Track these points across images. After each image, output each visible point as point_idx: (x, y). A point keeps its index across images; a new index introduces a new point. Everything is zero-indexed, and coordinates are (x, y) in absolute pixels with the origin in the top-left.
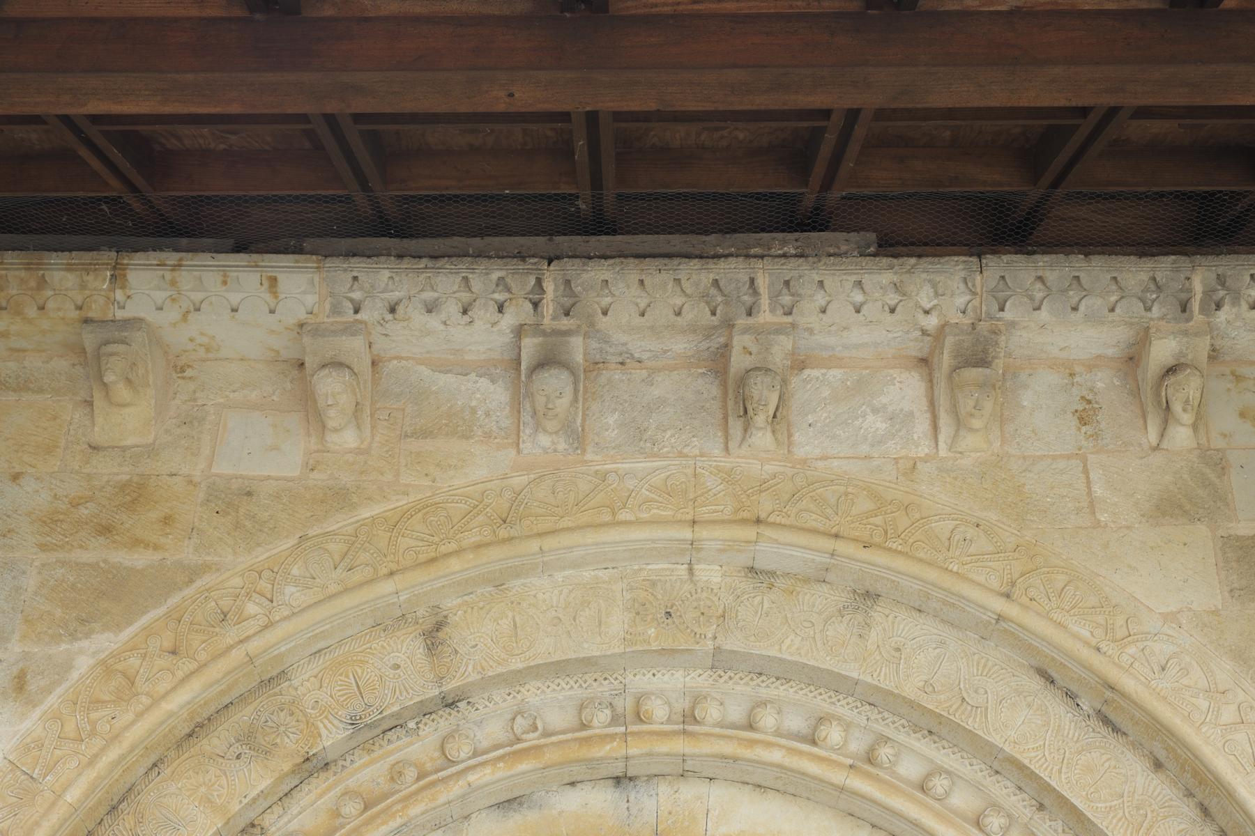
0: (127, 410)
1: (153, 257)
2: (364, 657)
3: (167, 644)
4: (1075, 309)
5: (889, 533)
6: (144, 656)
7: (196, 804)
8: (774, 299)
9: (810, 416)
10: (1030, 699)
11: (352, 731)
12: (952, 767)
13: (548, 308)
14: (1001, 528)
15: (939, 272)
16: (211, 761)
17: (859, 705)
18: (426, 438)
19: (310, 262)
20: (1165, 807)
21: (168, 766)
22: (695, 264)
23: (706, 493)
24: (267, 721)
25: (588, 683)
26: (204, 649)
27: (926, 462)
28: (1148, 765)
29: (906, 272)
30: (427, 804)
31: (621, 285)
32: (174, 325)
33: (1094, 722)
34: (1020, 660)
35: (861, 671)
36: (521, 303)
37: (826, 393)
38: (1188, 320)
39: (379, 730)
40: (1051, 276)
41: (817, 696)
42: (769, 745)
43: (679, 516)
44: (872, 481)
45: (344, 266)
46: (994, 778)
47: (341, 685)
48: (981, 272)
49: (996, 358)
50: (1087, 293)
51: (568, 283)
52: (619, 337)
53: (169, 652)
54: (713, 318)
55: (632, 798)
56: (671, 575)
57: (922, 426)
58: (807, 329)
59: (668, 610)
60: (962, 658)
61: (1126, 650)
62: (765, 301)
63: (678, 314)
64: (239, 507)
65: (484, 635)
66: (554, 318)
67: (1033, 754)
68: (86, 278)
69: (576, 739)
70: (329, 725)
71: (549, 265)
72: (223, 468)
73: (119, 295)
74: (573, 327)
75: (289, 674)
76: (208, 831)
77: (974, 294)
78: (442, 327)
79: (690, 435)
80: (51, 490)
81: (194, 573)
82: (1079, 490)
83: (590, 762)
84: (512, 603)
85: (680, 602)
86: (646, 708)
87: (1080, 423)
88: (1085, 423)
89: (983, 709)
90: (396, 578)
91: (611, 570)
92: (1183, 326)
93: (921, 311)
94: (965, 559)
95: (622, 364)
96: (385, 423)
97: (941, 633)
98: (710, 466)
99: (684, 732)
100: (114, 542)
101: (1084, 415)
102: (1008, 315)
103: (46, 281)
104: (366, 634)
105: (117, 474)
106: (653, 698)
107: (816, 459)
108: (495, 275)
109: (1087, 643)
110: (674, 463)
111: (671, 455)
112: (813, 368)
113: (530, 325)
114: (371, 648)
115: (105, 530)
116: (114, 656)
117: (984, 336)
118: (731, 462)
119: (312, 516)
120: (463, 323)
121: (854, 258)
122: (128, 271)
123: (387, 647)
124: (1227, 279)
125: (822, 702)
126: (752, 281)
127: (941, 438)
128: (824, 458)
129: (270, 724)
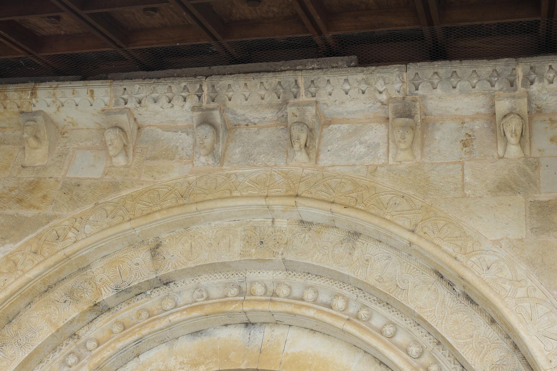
0: (38, 151)
1: (48, 84)
2: (124, 259)
3: (33, 249)
4: (454, 88)
5: (358, 201)
6: (23, 254)
7: (44, 321)
8: (307, 89)
9: (329, 147)
10: (430, 285)
11: (116, 293)
12: (396, 321)
13: (205, 98)
14: (415, 198)
15: (385, 72)
16: (53, 303)
17: (354, 289)
18: (155, 160)
19: (107, 83)
20: (495, 343)
21: (34, 304)
22: (270, 75)
23: (274, 183)
24: (79, 287)
25: (229, 276)
26: (47, 252)
27: (382, 167)
28: (487, 321)
29: (369, 74)
30: (150, 329)
31: (237, 86)
32: (55, 113)
33: (461, 298)
34: (427, 266)
35: (349, 271)
36: (193, 96)
37: (339, 135)
38: (515, 90)
39: (132, 294)
40: (441, 71)
41: (312, 279)
42: (309, 307)
43: (261, 194)
44: (354, 176)
45: (121, 84)
46: (416, 328)
47: (113, 272)
48: (406, 72)
49: (416, 114)
50: (460, 79)
51: (213, 86)
52: (240, 111)
53: (33, 253)
54: (279, 100)
55: (252, 333)
56: (264, 224)
57: (382, 150)
58: (324, 104)
59: (261, 241)
60: (398, 265)
61: (471, 259)
62: (302, 91)
63: (263, 99)
64: (73, 191)
65: (177, 251)
66: (208, 103)
67: (429, 314)
68: (22, 94)
69: (219, 302)
70: (106, 290)
71: (206, 79)
72: (70, 175)
73: (34, 101)
74: (216, 107)
75: (91, 266)
76: (48, 334)
77: (403, 82)
78: (161, 110)
79: (272, 156)
80: (3, 184)
81: (50, 219)
82: (458, 179)
83: (231, 314)
84: (191, 236)
85: (267, 237)
86: (253, 288)
87: (463, 146)
88: (466, 146)
89: (407, 290)
90: (131, 221)
91: (237, 222)
92: (512, 94)
93: (378, 92)
94: (394, 213)
95: (247, 125)
96: (139, 154)
97: (389, 252)
98: (279, 170)
99: (271, 301)
100: (22, 206)
101: (466, 142)
102: (420, 92)
103: (7, 96)
104: (126, 249)
105: (29, 178)
106: (257, 283)
107: (329, 167)
108: (183, 84)
109: (450, 255)
110: (262, 169)
111: (261, 166)
112: (334, 124)
113: (197, 106)
114: (127, 255)
115: (20, 201)
116: (12, 254)
117: (408, 103)
118: (288, 169)
119: (102, 195)
120: (169, 107)
121: (345, 68)
122: (37, 91)
123: (134, 255)
124: (536, 68)
125: (336, 288)
126: (296, 81)
127: (390, 155)
128: (333, 166)
129: (80, 288)
